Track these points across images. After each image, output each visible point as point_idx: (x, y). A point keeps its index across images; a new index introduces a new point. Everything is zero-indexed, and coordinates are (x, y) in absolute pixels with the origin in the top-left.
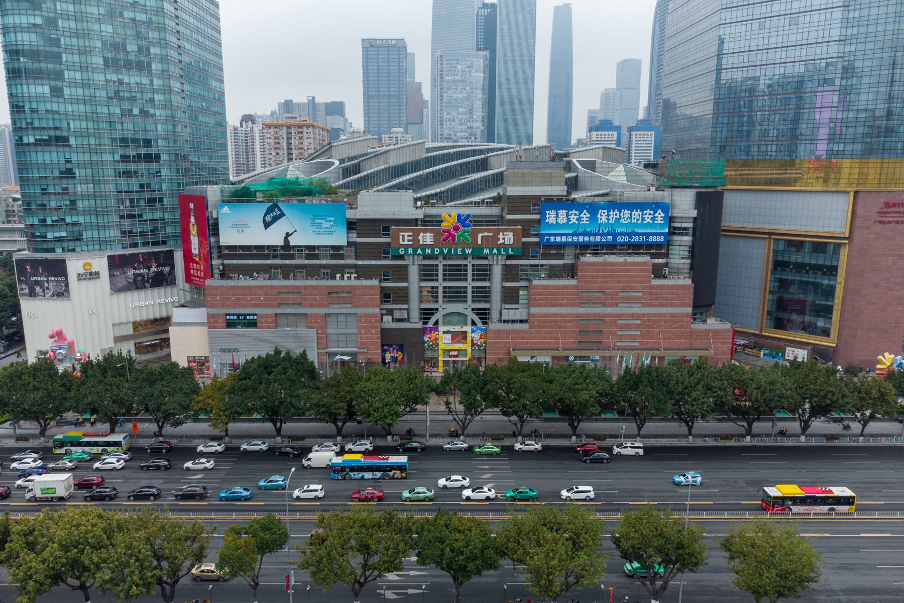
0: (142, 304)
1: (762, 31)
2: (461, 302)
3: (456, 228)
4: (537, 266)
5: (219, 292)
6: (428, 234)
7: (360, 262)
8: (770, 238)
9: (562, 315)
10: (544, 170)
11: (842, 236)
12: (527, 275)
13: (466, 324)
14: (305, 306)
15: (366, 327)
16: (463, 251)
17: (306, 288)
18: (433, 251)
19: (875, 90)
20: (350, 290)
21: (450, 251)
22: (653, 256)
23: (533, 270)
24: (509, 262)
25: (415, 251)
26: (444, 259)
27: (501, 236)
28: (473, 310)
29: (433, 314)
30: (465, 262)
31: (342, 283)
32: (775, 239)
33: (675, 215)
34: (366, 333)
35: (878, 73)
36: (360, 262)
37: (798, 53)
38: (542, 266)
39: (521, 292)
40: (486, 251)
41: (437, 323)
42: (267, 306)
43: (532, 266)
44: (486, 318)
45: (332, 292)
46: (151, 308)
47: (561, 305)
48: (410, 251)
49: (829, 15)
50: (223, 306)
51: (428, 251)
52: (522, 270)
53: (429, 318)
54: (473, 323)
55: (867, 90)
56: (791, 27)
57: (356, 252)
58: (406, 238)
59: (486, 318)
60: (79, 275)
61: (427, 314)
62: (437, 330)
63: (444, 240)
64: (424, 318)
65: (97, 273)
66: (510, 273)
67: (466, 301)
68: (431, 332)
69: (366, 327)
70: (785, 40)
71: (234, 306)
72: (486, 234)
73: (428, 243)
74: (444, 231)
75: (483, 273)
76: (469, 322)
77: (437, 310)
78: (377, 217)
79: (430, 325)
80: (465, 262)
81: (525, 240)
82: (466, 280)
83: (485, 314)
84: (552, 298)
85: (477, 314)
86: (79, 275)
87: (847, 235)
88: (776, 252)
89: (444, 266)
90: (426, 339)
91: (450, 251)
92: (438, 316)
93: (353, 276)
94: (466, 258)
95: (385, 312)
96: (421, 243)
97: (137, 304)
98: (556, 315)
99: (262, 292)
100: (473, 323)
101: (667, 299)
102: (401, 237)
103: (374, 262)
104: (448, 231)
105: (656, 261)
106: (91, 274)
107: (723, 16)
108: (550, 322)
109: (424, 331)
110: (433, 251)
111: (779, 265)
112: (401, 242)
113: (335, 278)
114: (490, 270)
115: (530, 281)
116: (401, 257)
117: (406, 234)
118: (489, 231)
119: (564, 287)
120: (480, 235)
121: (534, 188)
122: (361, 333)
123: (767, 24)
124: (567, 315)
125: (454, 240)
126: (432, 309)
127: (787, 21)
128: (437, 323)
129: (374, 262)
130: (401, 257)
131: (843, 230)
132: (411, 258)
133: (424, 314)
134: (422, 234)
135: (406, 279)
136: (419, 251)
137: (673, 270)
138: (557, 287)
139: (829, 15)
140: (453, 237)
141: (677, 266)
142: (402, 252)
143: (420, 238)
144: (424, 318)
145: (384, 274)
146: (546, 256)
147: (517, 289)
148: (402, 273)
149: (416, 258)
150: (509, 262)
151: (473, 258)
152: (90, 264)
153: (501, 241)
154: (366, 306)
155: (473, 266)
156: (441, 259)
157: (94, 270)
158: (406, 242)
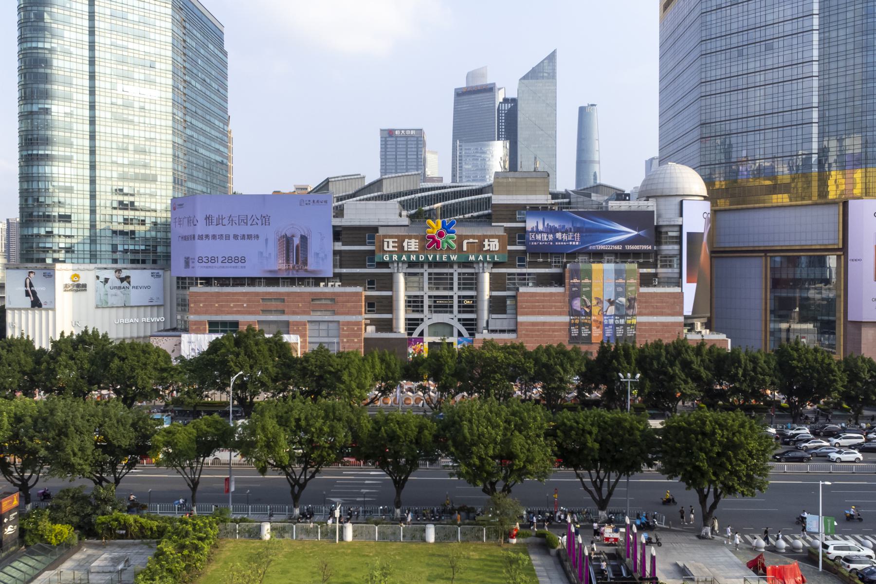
0: (127, 321)
1: (740, 58)
2: (446, 312)
3: (441, 235)
4: (524, 274)
5: (202, 298)
6: (413, 241)
7: (344, 271)
8: (766, 256)
9: (550, 324)
10: (528, 180)
11: (836, 247)
12: (514, 284)
13: (452, 335)
14: (288, 314)
15: (347, 336)
16: (449, 257)
17: (289, 294)
18: (418, 257)
19: (852, 104)
20: (333, 298)
21: (435, 257)
22: (641, 266)
23: (520, 279)
24: (495, 270)
25: (400, 258)
26: (430, 266)
27: (486, 243)
28: (459, 320)
29: (418, 325)
30: (451, 271)
31: (326, 290)
32: (771, 257)
33: (661, 223)
34: (348, 342)
35: (852, 88)
36: (344, 271)
37: (776, 75)
38: (529, 274)
39: (508, 302)
40: (472, 258)
41: (422, 334)
42: (249, 313)
43: (519, 274)
44: (472, 330)
45: (315, 297)
46: (135, 326)
47: (549, 314)
48: (395, 257)
49: (800, 39)
50: (206, 313)
51: (413, 258)
52: (509, 279)
53: (414, 329)
54: (460, 334)
55: (844, 105)
56: (767, 52)
57: (341, 260)
58: (391, 244)
59: (472, 330)
60: (66, 286)
61: (412, 325)
62: (422, 341)
63: (429, 247)
64: (409, 329)
65: (85, 286)
66: (497, 282)
67: (452, 312)
68: (415, 344)
69: (347, 336)
70: (728, 28)
71: (217, 314)
72: (471, 240)
73: (413, 249)
74: (429, 237)
75: (471, 282)
76: (456, 333)
77: (422, 320)
78: (362, 224)
79: (415, 335)
80: (451, 271)
81: (509, 248)
82: (452, 289)
83: (472, 324)
84: (541, 306)
85: (464, 325)
86: (66, 286)
87: (841, 246)
88: (773, 269)
89: (430, 274)
90: (410, 350)
91: (435, 257)
92: (424, 326)
93: (337, 284)
94: (452, 267)
95: (368, 322)
96: (406, 249)
97: (122, 320)
98: (544, 324)
99: (245, 298)
100: (460, 334)
101: (657, 308)
102: (386, 244)
103: (358, 270)
104: (433, 237)
105: (645, 271)
106: (78, 286)
107: (704, 47)
108: (539, 331)
109: (410, 342)
110: (418, 257)
111: (776, 283)
112: (386, 248)
113: (319, 285)
114: (476, 279)
115: (518, 289)
116: (385, 265)
117: (391, 240)
118: (473, 237)
119: (551, 294)
120: (465, 242)
121: (519, 197)
122: (343, 342)
123: (745, 52)
124: (555, 324)
125: (438, 246)
126: (417, 320)
127: (763, 48)
128: (422, 334)
129: (358, 270)
130: (385, 265)
131: (836, 241)
132: (396, 265)
133: (409, 324)
134: (406, 240)
135: (390, 288)
136: (404, 258)
137: (662, 280)
138: (544, 295)
139: (800, 39)
140: (438, 243)
141: (664, 275)
142: (386, 258)
143: (405, 244)
144: (409, 329)
145: (371, 282)
146: (533, 264)
147: (504, 298)
148: (388, 282)
149: (400, 265)
150: (495, 270)
151: (459, 267)
152: (78, 276)
153: (486, 248)
154: (348, 313)
155: (459, 274)
156: (426, 267)
157: (81, 282)
158: (391, 249)
